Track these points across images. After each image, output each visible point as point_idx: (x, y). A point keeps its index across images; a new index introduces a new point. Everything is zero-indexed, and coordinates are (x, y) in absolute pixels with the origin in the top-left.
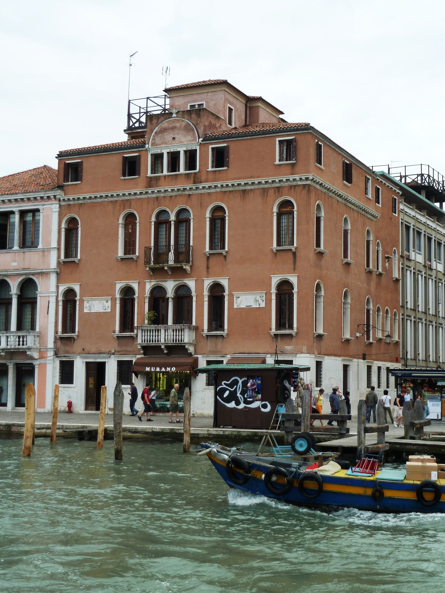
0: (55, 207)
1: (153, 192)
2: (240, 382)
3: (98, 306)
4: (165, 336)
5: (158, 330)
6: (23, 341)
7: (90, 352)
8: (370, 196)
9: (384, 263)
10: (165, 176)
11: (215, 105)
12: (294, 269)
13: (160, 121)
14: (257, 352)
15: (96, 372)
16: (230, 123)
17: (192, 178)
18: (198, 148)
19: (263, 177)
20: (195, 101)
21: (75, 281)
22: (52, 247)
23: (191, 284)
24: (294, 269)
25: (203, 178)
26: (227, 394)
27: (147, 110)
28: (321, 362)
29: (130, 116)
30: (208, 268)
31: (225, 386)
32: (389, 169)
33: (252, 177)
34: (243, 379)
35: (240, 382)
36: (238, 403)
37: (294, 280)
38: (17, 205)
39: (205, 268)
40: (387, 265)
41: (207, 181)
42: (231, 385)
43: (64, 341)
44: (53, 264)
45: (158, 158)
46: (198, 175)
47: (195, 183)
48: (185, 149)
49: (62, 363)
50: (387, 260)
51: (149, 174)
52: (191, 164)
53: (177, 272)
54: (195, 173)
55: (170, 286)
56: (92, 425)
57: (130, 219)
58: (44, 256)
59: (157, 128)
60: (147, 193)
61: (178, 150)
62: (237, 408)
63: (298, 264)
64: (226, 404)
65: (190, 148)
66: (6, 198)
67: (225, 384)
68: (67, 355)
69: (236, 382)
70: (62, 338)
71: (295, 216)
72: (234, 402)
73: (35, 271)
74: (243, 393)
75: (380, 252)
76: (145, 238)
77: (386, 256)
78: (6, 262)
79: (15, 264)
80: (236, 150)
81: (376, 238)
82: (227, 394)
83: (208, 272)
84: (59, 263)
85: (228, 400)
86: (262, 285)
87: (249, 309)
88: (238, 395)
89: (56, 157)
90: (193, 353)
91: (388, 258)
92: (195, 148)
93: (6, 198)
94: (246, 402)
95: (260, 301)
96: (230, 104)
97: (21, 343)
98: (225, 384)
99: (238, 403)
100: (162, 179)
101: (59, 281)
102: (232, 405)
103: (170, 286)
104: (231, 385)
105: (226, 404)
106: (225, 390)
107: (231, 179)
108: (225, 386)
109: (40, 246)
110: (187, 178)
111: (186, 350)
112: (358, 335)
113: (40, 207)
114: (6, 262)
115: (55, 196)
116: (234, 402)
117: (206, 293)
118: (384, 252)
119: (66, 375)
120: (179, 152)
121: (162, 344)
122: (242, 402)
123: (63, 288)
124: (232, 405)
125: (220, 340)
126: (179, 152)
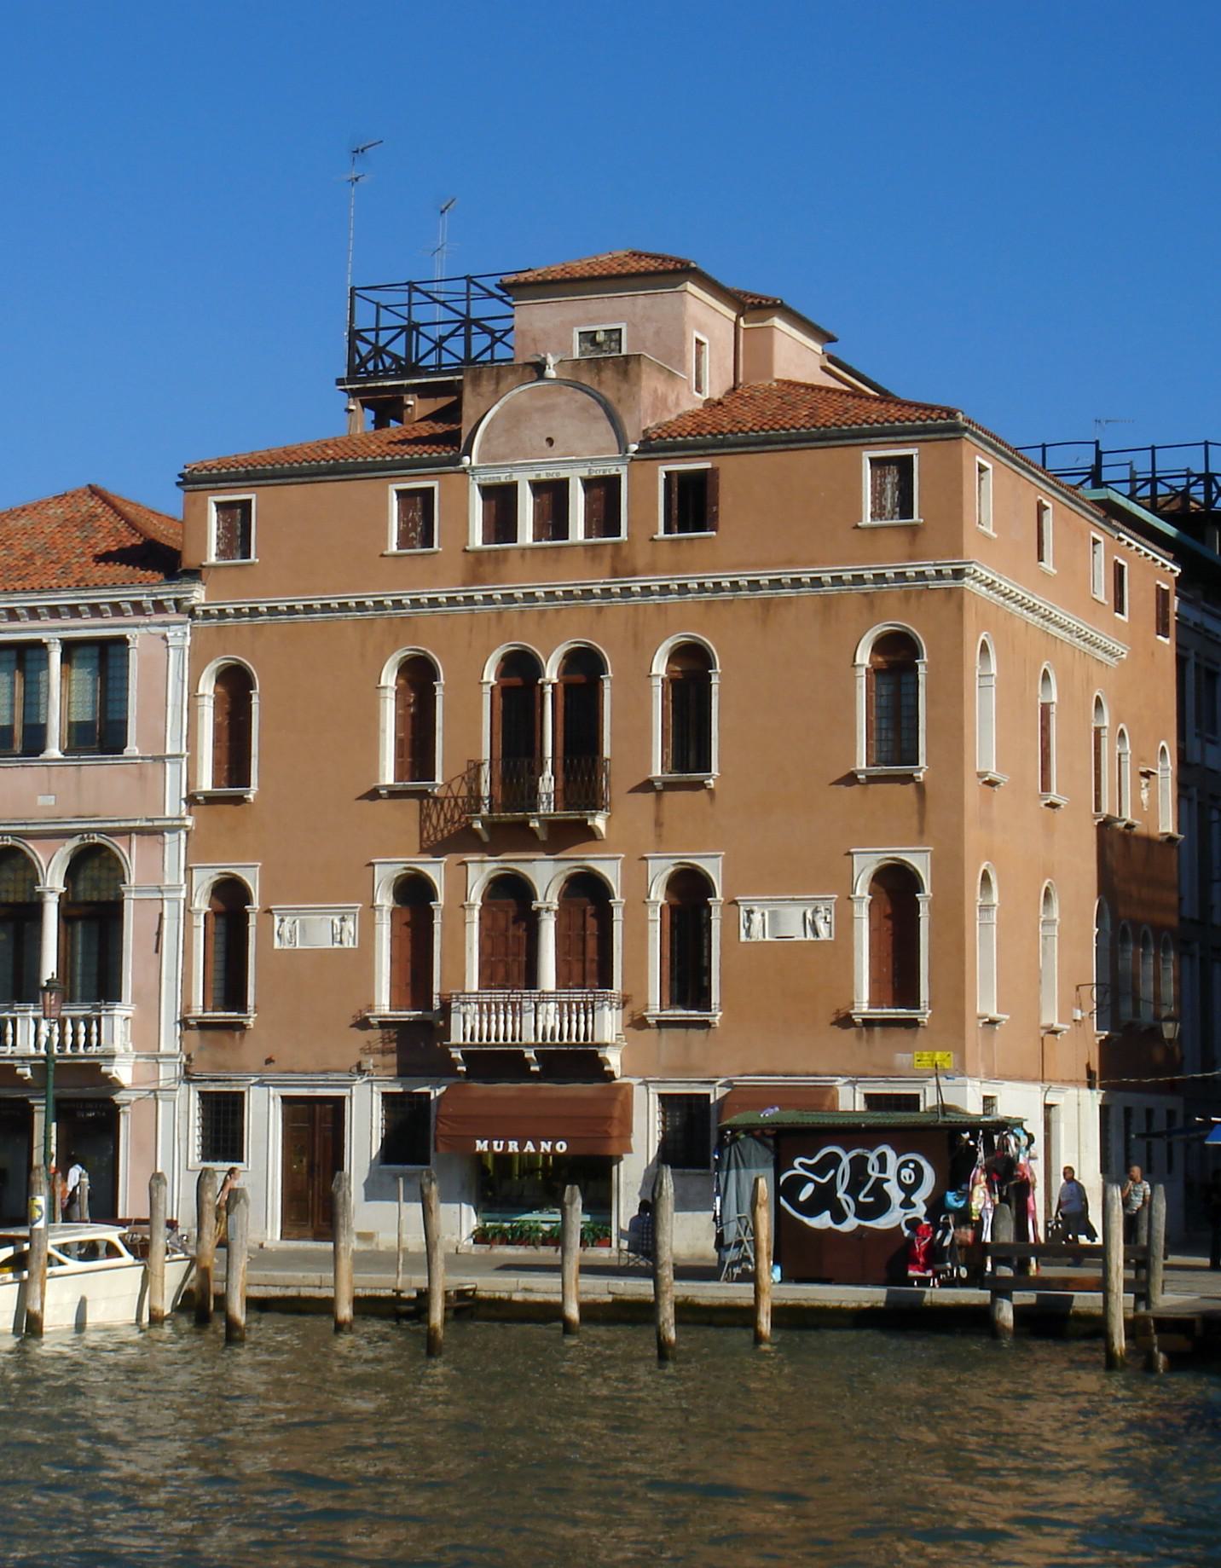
0: (180, 635)
1: (488, 599)
2: (846, 1159)
3: (327, 931)
4: (543, 1020)
5: (513, 1004)
6: (88, 1034)
7: (296, 1068)
8: (1101, 597)
9: (1137, 789)
10: (524, 549)
11: (657, 333)
12: (921, 832)
13: (503, 386)
14: (811, 1070)
15: (315, 1130)
16: (699, 389)
17: (607, 561)
18: (623, 471)
19: (824, 564)
20: (592, 321)
21: (241, 855)
22: (169, 752)
23: (610, 871)
24: (921, 832)
25: (641, 561)
26: (807, 1192)
27: (408, 319)
28: (242, 1093)
29: (355, 335)
30: (658, 824)
31: (802, 1172)
32: (1099, 454)
33: (790, 563)
34: (853, 1153)
35: (846, 1159)
36: (839, 1216)
37: (921, 863)
38: (56, 623)
39: (651, 826)
40: (1144, 795)
41: (652, 569)
42: (820, 1169)
43: (209, 1034)
44: (173, 806)
45: (501, 499)
46: (625, 552)
47: (615, 573)
48: (585, 473)
49: (203, 1095)
50: (1144, 781)
51: (477, 540)
52: (605, 517)
53: (569, 833)
54: (616, 544)
55: (546, 876)
56: (306, 1282)
57: (419, 676)
58: (142, 776)
59: (496, 408)
60: (469, 600)
61: (563, 474)
62: (837, 1231)
63: (931, 817)
64: (806, 1220)
65: (599, 471)
66: (20, 602)
67: (801, 1164)
68: (221, 1075)
69: (833, 1161)
70: (203, 1026)
71: (921, 678)
72: (827, 1213)
73: (116, 825)
74: (853, 1190)
75: (1127, 759)
76: (469, 732)
77: (1144, 770)
78: (30, 799)
79: (50, 800)
80: (738, 478)
81: (1117, 718)
82: (807, 1192)
83: (659, 836)
84: (191, 800)
85: (811, 1208)
86: (820, 875)
87: (784, 948)
88: (840, 1195)
89: (178, 484)
90: (618, 1074)
91: (1147, 775)
92: (613, 472)
93: (20, 602)
94: (864, 1212)
95: (821, 925)
96: (700, 330)
97: (82, 1039)
98: (801, 1164)
99: (839, 1216)
100: (514, 558)
101: (197, 853)
102: (823, 1221)
103: (546, 876)
104: (820, 1169)
105: (806, 1220)
106: (803, 1181)
107: (716, 558)
108: (802, 1172)
109: (132, 749)
110: (593, 559)
111: (602, 1062)
112: (1078, 1015)
113: (129, 633)
114: (30, 799)
115: (177, 602)
116: (827, 1213)
117: (658, 895)
118: (1138, 759)
119: (223, 1130)
120: (564, 483)
121: (528, 1046)
122: (851, 1215)
123: (205, 879)
124: (823, 1221)
125: (696, 1035)
126: (564, 483)
